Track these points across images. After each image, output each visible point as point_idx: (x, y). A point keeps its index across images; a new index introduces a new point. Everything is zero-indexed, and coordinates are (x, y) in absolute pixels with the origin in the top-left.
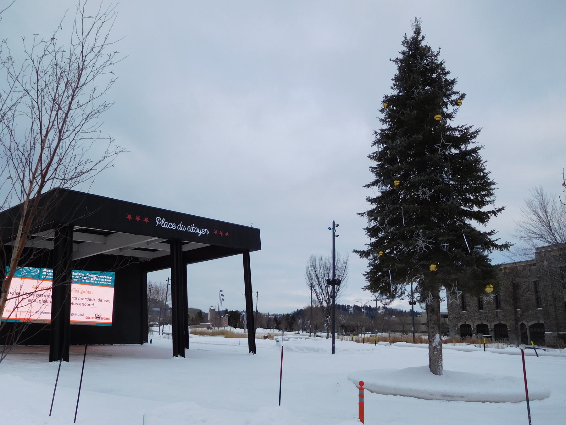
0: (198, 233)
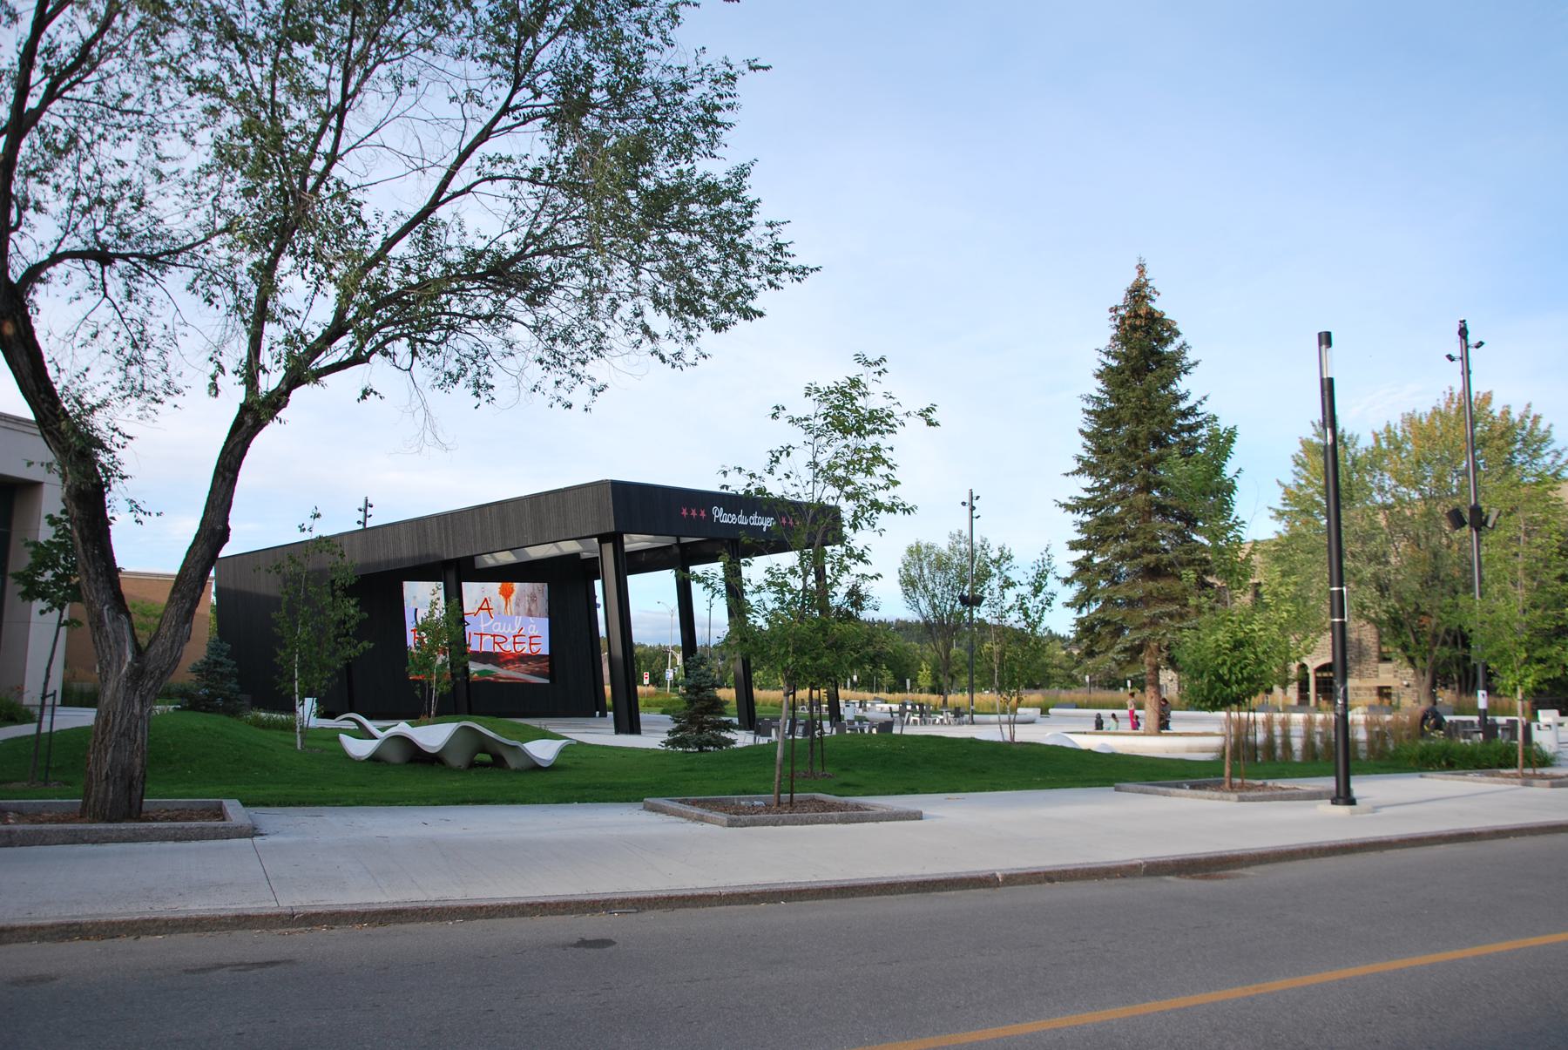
0: (762, 526)
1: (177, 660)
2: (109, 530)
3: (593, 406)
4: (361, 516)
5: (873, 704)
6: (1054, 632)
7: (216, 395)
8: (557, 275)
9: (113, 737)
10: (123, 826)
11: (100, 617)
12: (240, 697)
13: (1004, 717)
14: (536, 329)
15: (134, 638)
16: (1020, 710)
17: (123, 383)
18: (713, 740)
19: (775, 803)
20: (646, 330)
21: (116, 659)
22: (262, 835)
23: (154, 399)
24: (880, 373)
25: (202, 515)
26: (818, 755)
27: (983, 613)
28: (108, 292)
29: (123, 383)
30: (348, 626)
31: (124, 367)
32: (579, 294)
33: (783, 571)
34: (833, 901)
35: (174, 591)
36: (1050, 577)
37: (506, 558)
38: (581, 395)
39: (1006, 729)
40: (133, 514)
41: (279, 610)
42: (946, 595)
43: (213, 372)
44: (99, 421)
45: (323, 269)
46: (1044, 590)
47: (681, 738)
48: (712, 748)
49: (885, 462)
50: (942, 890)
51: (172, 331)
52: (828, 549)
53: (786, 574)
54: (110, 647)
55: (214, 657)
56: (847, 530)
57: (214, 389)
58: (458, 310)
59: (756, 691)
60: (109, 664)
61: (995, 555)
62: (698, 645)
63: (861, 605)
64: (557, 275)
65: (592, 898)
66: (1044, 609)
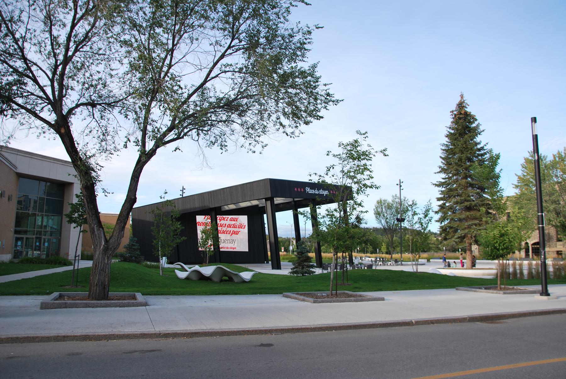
0: (324, 194)
1: (119, 244)
3: (263, 152)
4: (181, 193)
5: (365, 258)
6: (431, 231)
8: (249, 105)
10: (102, 302)
11: (93, 229)
12: (141, 257)
13: (414, 263)
14: (242, 125)
18: (307, 271)
19: (331, 294)
21: (99, 244)
22: (149, 305)
23: (110, 153)
24: (365, 138)
27: (405, 224)
28: (95, 116)
30: (177, 231)
32: (257, 112)
33: (332, 210)
34: (352, 330)
35: (118, 220)
37: (232, 207)
38: (258, 148)
39: (415, 267)
40: (104, 193)
41: (154, 226)
44: (92, 161)
45: (167, 106)
46: (428, 216)
47: (296, 271)
48: (307, 274)
49: (368, 170)
50: (392, 327)
51: (116, 129)
52: (348, 202)
55: (132, 243)
56: (355, 195)
58: (214, 119)
59: (322, 254)
60: (97, 245)
61: (410, 203)
63: (360, 222)
64: (249, 105)
65: (265, 329)
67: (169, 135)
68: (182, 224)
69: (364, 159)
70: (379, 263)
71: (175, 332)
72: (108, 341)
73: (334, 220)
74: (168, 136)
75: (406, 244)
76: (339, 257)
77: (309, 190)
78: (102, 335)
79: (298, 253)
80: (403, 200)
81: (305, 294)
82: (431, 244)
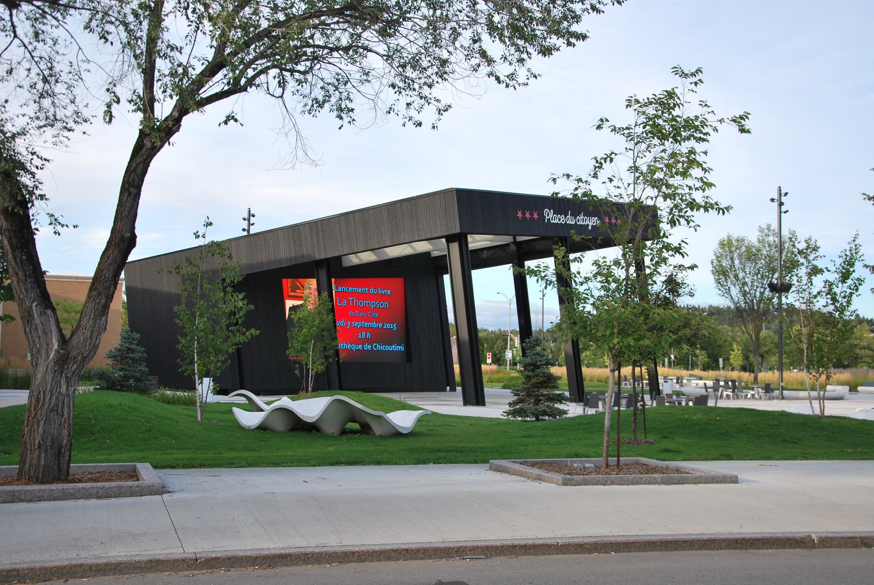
0: (588, 225)
1: (96, 347)
2: (34, 239)
3: (439, 124)
4: (245, 224)
5: (689, 380)
6: (861, 316)
7: (110, 120)
8: (405, 8)
9: (44, 412)
10: (53, 487)
11: (30, 313)
12: (149, 377)
13: (814, 394)
14: (388, 58)
15: (60, 330)
16: (828, 387)
17: (38, 114)
18: (548, 410)
19: (604, 465)
20: (483, 54)
21: (45, 347)
22: (169, 492)
23: (66, 128)
24: (696, 84)
25: (112, 225)
26: (640, 424)
27: (791, 299)
28: (18, 33)
29: (38, 114)
30: (237, 316)
31: (37, 100)
32: (424, 24)
33: (608, 264)
34: (658, 553)
35: (91, 289)
36: (858, 265)
37: (368, 257)
38: (428, 114)
39: (816, 404)
40: (52, 226)
41: (180, 304)
42: (755, 283)
43: (108, 101)
44: (20, 145)
45: (203, 9)
46: (851, 277)
47: (521, 409)
48: (547, 418)
49: (699, 165)
50: (759, 548)
51: (76, 67)
52: (648, 243)
53: (610, 266)
54: (39, 337)
55: (127, 345)
56: (664, 226)
57: (109, 116)
58: (321, 43)
59: (584, 369)
60: (39, 351)
61: (802, 246)
62: (533, 329)
63: (677, 292)
64: (405, 8)
65: (447, 545)
66: (851, 294)
67: (210, 83)
68: (249, 299)
69: (688, 139)
70: (725, 393)
71: (234, 554)
72: (67, 580)
73: (613, 286)
74: (207, 86)
75: (794, 346)
76: (625, 376)
77: (551, 216)
78: (51, 568)
79: (525, 367)
80: (787, 240)
81: (543, 463)
82: (861, 349)
